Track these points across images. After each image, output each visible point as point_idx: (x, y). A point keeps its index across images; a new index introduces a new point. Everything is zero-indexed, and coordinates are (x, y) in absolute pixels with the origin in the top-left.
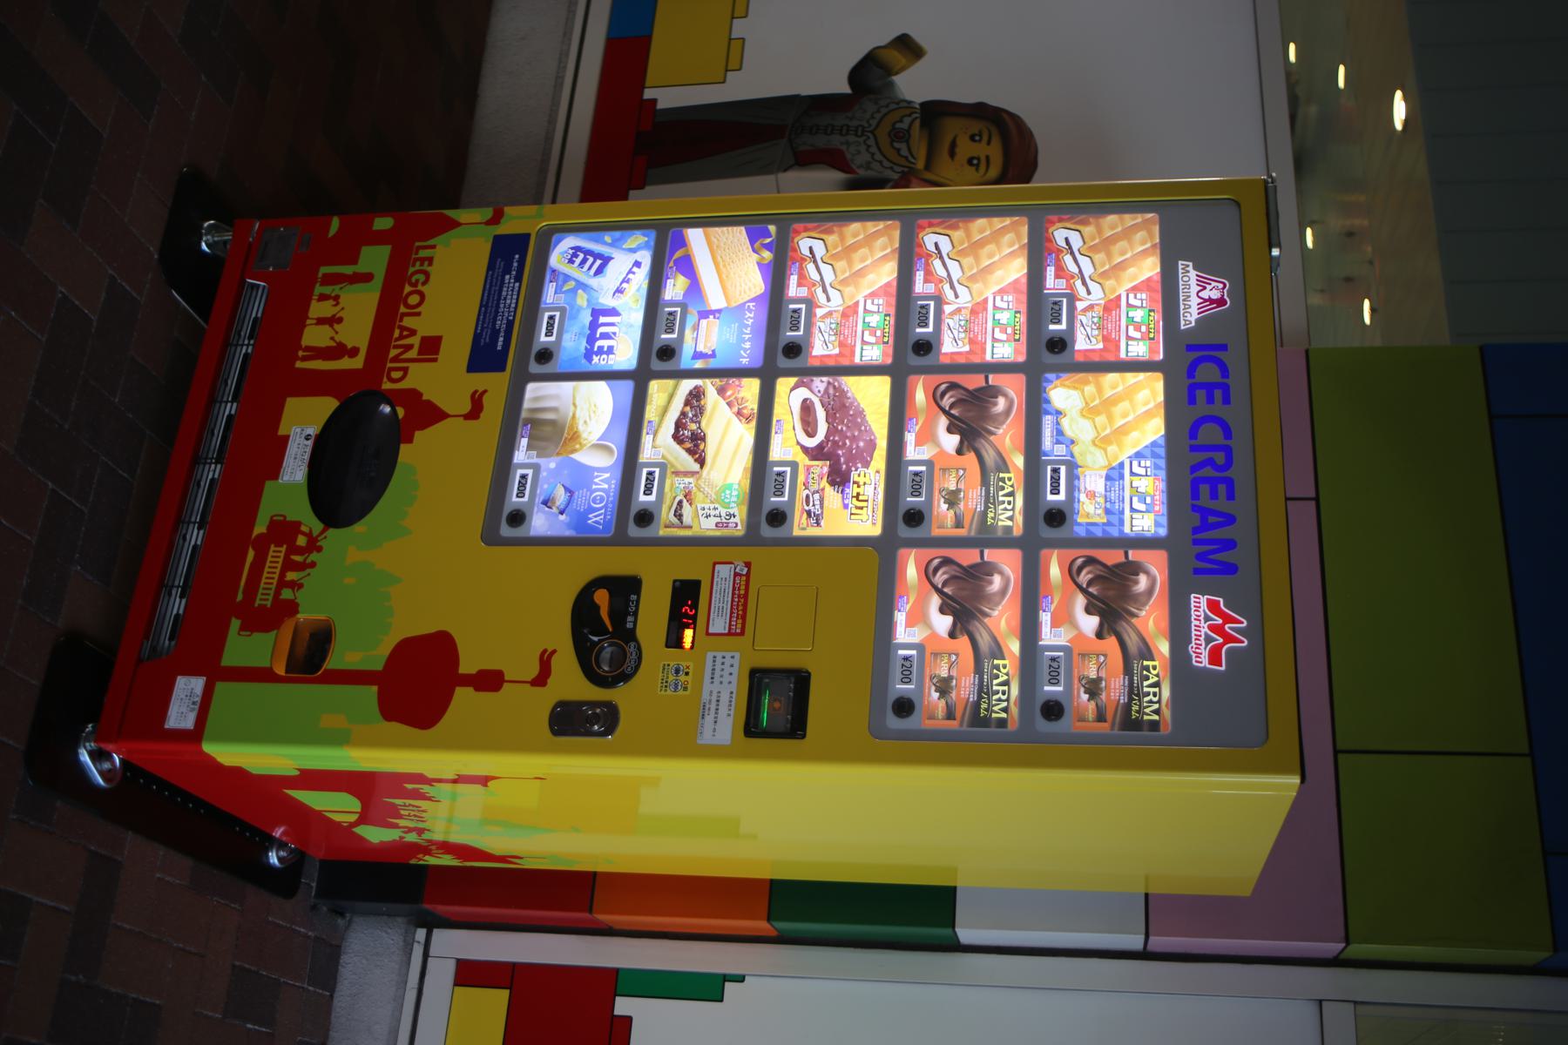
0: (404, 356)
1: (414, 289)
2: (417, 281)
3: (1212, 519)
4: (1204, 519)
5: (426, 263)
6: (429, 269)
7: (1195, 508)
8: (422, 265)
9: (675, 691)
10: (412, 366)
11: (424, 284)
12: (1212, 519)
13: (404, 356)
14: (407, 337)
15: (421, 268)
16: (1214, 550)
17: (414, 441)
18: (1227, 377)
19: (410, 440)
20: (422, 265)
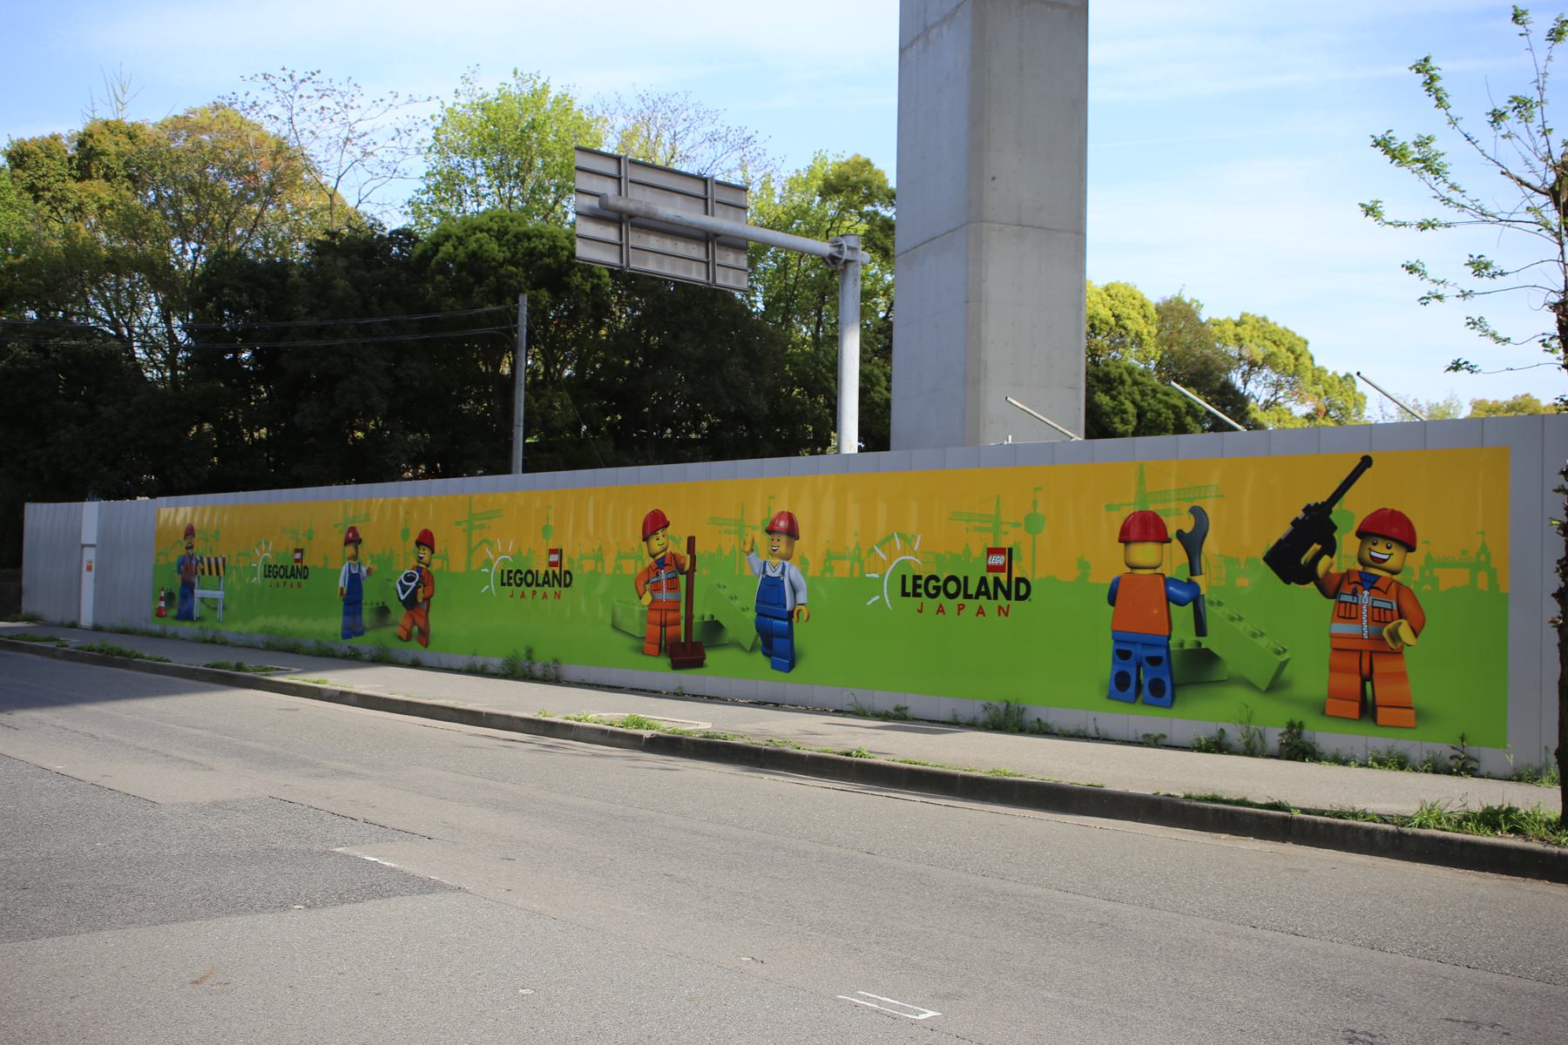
0: (1005, 585)
1: (942, 591)
2: (935, 587)
3: (983, 589)
4: (983, 594)
5: (919, 582)
6: (924, 578)
7: (977, 597)
8: (920, 586)
9: (1142, 465)
10: (1015, 575)
11: (937, 579)
12: (983, 589)
13: (1005, 585)
14: (987, 587)
15: (923, 587)
16: (891, 726)
17: (675, 671)
18: (1004, 549)
19: (1317, 504)
20: (920, 586)
